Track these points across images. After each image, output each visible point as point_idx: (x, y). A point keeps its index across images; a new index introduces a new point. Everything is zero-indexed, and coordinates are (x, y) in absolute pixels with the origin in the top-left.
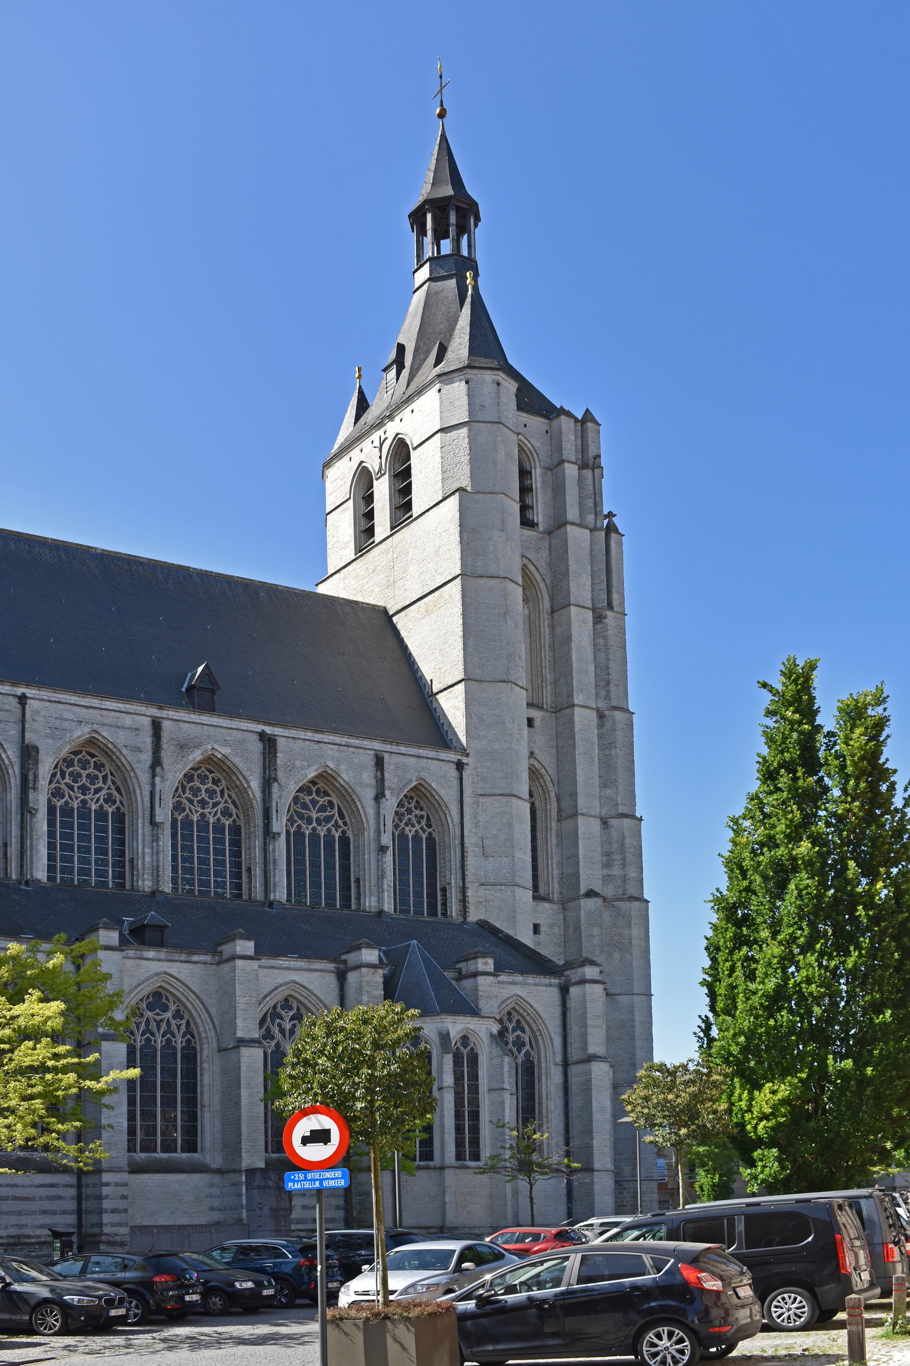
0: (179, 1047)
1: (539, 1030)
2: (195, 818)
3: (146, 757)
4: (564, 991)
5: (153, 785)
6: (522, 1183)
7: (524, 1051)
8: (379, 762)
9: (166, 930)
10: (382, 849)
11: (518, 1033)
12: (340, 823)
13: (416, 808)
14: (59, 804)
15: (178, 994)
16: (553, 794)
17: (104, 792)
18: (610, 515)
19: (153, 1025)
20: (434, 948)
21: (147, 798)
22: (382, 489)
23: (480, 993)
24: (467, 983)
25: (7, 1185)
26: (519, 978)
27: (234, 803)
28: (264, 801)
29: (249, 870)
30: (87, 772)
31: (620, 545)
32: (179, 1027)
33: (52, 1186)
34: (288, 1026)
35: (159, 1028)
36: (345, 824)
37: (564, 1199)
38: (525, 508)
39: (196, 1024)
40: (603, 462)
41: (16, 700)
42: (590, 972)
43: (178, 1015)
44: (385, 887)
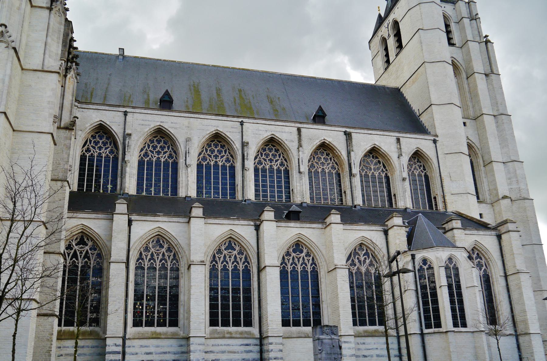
0: (309, 271)
1: (489, 258)
3: (296, 144)
4: (499, 237)
5: (299, 155)
6: (493, 340)
7: (483, 270)
8: (398, 140)
9: (301, 215)
10: (404, 179)
11: (479, 260)
12: (384, 170)
13: (418, 162)
14: (260, 167)
15: (307, 244)
16: (479, 155)
18: (486, 36)
19: (296, 260)
20: (431, 217)
21: (297, 162)
22: (392, 43)
23: (456, 238)
24: (449, 234)
25: (225, 345)
26: (475, 232)
27: (336, 163)
28: (348, 160)
29: (345, 192)
31: (493, 47)
33: (247, 345)
34: (362, 259)
35: (299, 261)
36: (387, 170)
37: (516, 350)
38: (449, 39)
39: (316, 259)
40: (479, 16)
41: (239, 123)
42: (511, 226)
44: (407, 196)
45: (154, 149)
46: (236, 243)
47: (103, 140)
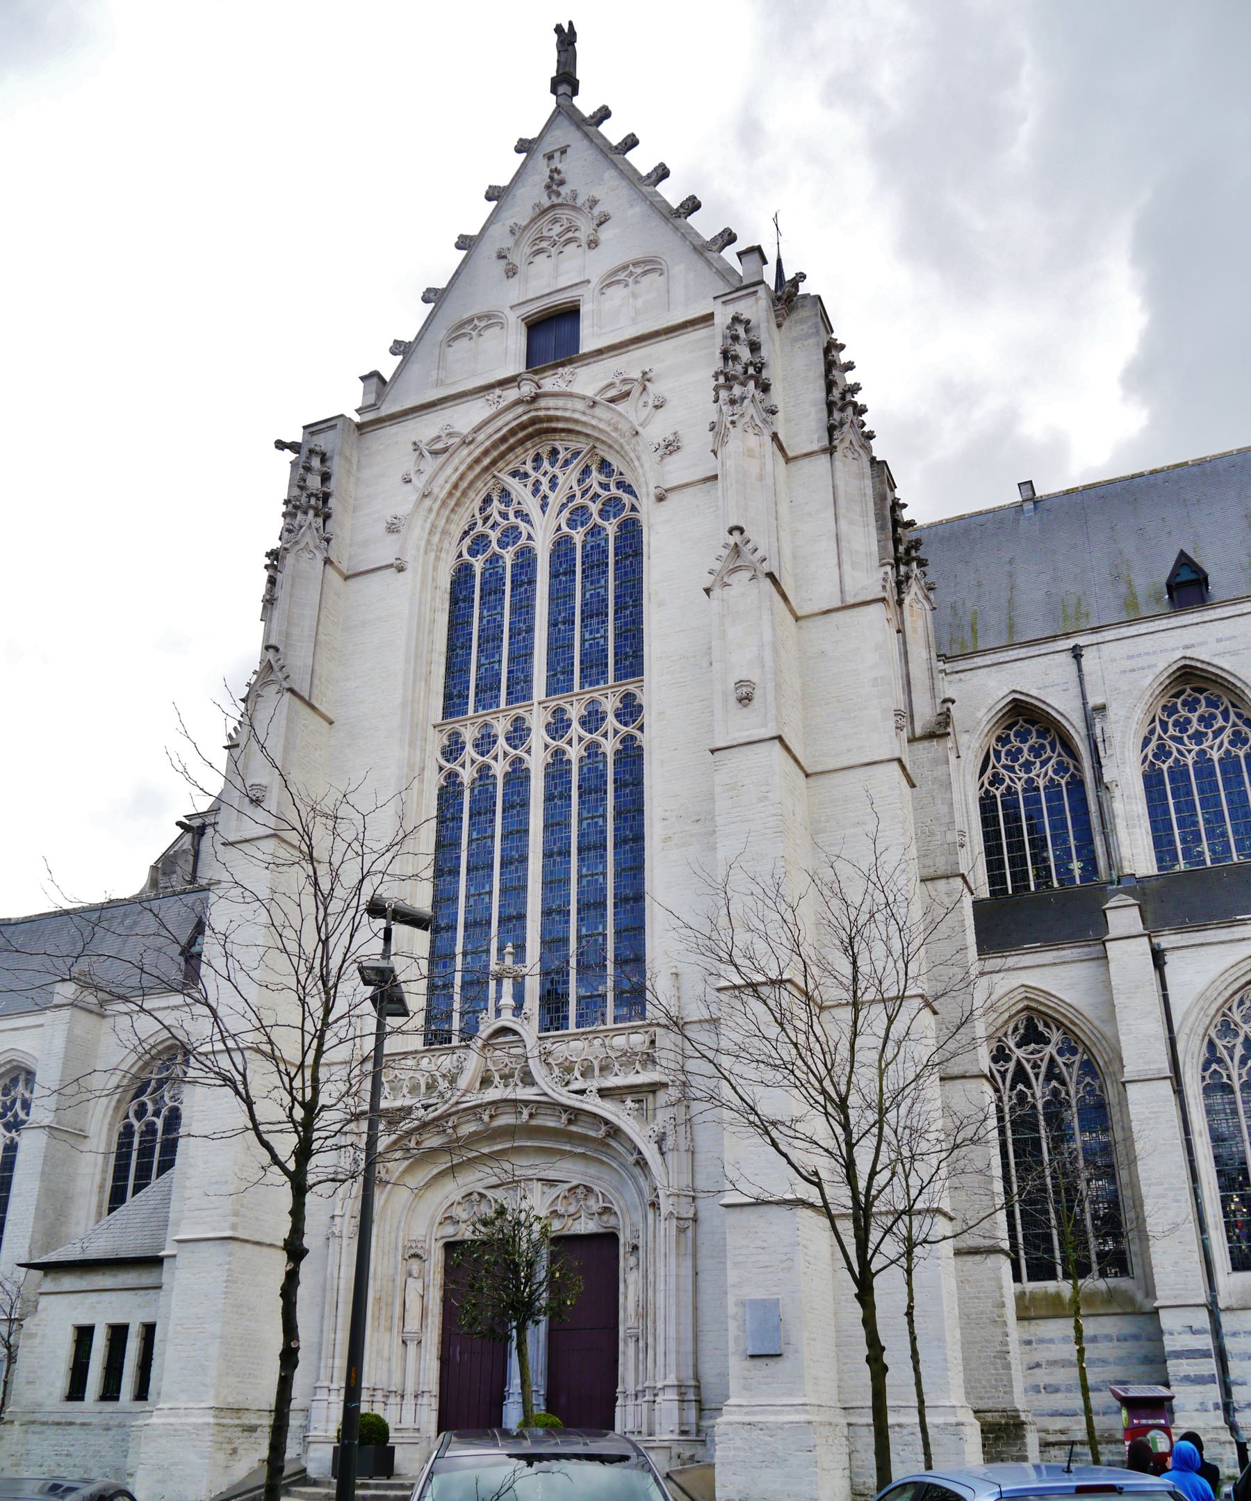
2: (1019, 786)
17: (1229, 731)
30: (1197, 714)
32: (1231, 1050)
43: (1068, 1048)
45: (1015, 760)
46: (1049, 1020)
47: (1031, 742)
